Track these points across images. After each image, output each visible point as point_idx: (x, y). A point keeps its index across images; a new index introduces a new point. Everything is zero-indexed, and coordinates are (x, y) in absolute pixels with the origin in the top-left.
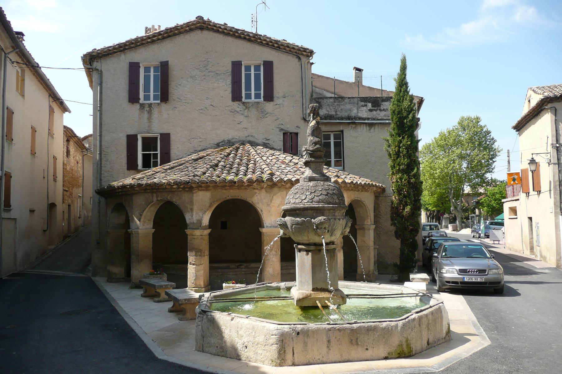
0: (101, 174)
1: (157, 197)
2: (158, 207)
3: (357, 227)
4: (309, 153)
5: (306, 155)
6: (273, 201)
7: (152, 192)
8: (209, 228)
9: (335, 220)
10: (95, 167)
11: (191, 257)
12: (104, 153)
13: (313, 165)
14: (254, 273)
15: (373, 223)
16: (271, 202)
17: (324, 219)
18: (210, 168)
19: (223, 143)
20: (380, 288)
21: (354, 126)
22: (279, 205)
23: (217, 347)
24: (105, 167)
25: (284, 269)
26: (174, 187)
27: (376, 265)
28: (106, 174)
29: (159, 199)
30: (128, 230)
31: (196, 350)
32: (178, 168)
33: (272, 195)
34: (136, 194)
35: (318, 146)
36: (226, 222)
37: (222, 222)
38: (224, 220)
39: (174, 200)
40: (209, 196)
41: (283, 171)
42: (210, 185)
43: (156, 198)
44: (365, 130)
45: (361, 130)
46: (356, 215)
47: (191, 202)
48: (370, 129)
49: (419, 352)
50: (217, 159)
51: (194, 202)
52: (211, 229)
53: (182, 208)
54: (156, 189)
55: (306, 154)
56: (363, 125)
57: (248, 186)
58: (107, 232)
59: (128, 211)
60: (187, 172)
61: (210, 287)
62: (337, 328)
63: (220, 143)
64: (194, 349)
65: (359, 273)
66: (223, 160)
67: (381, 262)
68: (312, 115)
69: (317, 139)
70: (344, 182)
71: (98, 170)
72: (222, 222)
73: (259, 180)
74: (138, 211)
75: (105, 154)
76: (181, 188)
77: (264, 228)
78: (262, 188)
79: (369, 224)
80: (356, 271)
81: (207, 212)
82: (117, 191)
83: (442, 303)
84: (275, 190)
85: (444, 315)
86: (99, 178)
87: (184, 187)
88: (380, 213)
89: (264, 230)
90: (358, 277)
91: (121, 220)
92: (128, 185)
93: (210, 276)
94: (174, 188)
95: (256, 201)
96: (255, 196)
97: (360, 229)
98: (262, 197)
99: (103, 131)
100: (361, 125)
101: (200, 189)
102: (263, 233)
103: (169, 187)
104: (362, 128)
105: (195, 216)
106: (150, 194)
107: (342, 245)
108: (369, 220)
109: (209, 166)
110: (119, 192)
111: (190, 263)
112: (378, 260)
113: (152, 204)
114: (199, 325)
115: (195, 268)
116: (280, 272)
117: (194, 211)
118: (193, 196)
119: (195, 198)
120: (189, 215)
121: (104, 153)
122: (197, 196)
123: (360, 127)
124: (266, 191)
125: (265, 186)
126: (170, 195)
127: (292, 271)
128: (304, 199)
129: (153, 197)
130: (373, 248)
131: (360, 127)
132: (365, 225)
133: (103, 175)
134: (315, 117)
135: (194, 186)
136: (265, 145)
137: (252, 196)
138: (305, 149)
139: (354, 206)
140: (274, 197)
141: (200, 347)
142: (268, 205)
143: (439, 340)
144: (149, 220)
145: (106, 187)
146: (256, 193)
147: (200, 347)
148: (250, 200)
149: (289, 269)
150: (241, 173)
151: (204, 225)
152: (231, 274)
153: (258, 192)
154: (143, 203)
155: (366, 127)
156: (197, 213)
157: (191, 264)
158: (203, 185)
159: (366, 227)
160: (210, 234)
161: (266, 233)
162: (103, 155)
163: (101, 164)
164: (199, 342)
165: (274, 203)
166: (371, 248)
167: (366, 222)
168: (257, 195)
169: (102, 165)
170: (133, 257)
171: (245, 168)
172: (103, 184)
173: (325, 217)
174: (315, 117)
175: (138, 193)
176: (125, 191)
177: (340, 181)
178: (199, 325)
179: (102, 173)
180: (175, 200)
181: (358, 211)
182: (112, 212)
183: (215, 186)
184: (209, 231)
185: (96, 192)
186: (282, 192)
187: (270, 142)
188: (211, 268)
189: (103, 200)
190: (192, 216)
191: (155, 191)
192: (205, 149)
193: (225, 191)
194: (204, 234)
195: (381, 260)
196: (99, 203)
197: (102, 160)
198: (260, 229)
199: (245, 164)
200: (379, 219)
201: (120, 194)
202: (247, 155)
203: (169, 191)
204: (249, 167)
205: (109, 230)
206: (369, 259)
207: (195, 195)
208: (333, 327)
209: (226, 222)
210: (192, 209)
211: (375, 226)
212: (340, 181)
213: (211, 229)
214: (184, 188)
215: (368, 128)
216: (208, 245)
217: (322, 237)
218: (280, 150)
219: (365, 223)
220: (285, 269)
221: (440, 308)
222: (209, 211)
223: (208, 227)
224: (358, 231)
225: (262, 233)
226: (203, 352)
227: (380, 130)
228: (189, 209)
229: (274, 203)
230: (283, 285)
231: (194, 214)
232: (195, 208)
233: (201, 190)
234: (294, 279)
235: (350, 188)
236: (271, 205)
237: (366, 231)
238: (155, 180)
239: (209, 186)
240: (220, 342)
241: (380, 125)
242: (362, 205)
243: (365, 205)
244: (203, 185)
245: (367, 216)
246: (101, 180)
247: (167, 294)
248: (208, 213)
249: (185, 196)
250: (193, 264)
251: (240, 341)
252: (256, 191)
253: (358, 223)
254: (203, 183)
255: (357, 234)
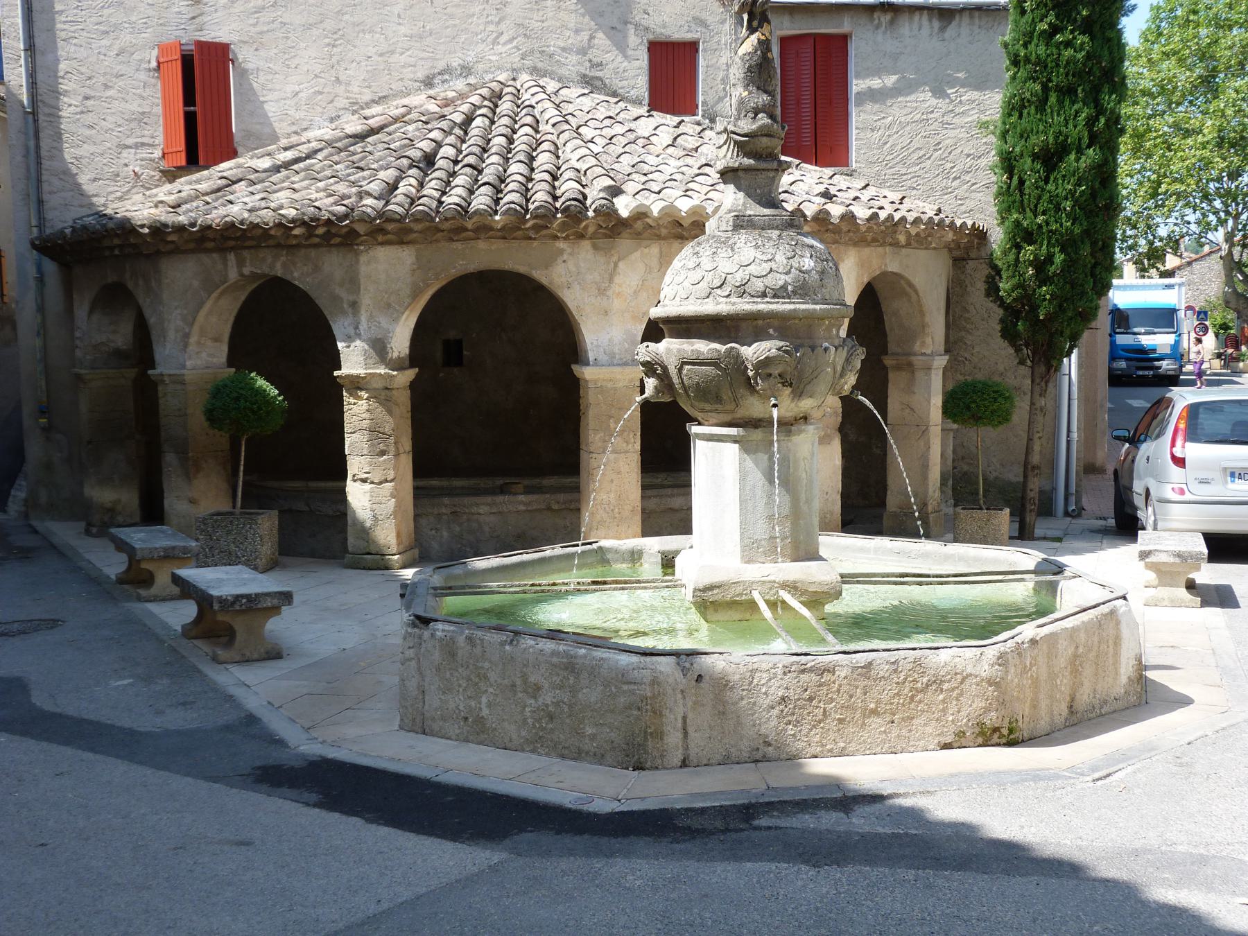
0: (39, 181)
1: (241, 263)
2: (243, 298)
3: (888, 361)
4: (736, 142)
5: (726, 146)
6: (617, 279)
7: (222, 250)
8: (412, 366)
9: (813, 351)
10: (19, 158)
11: (357, 458)
12: (47, 110)
13: (745, 179)
14: (555, 507)
15: (942, 349)
16: (611, 280)
17: (779, 349)
18: (411, 166)
19: (446, 77)
20: (947, 558)
21: (888, 17)
22: (635, 292)
23: (466, 719)
24: (52, 158)
25: (650, 497)
26: (296, 232)
27: (950, 482)
28: (55, 181)
29: (246, 271)
30: (150, 372)
31: (401, 728)
32: (301, 165)
33: (615, 259)
34: (171, 253)
35: (763, 119)
36: (459, 343)
37: (447, 343)
38: (452, 334)
39: (296, 274)
40: (409, 262)
41: (650, 176)
42: (412, 225)
43: (235, 270)
44: (926, 31)
45: (911, 30)
46: (887, 324)
47: (353, 283)
48: (943, 29)
49: (1043, 733)
50: (431, 135)
51: (362, 281)
52: (417, 370)
53: (322, 302)
54: (236, 239)
55: (725, 143)
56: (921, 15)
57: (536, 228)
58: (78, 377)
59: (147, 313)
60: (332, 180)
61: (416, 551)
62: (809, 665)
63: (434, 76)
64: (397, 727)
65: (893, 510)
66: (451, 139)
67: (965, 473)
68: (746, 17)
69: (763, 98)
70: (849, 217)
71: (28, 170)
72: (447, 343)
73: (572, 208)
74: (178, 311)
75: (50, 115)
76: (317, 236)
77: (588, 364)
78: (581, 236)
79: (929, 352)
80: (883, 504)
81: (405, 316)
82: (106, 243)
83: (1124, 598)
84: (624, 243)
85: (1125, 632)
86: (33, 198)
87: (328, 231)
88: (967, 315)
89: (587, 373)
90: (886, 522)
91: (121, 336)
92: (143, 226)
93: (416, 517)
94: (296, 236)
95: (563, 279)
96: (559, 261)
97: (899, 368)
98: (582, 265)
99: (36, 34)
100: (914, 12)
101: (380, 238)
102: (586, 381)
103: (279, 234)
104: (915, 26)
105: (365, 326)
106: (215, 255)
107: (840, 419)
108: (929, 340)
109: (405, 162)
110: (112, 248)
111: (354, 476)
112: (954, 468)
113: (222, 288)
114: (410, 660)
115: (372, 491)
116: (639, 504)
117: (363, 312)
118: (358, 261)
119: (363, 269)
120: (346, 323)
121: (47, 110)
122: (369, 262)
123: (911, 19)
124: (595, 247)
125: (591, 230)
126: (283, 258)
127: (677, 502)
128: (720, 287)
129: (226, 265)
130: (939, 428)
131: (911, 19)
132: (915, 355)
133: (45, 187)
134: (755, 24)
135: (361, 228)
136: (587, 83)
137: (548, 264)
138: (722, 129)
139: (882, 293)
140: (621, 265)
141: (414, 720)
142: (602, 292)
143: (1106, 702)
144: (216, 340)
145: (68, 231)
146: (561, 252)
147: (414, 720)
148: (540, 276)
149: (669, 496)
150: (512, 186)
151: (395, 355)
152: (481, 511)
153: (569, 250)
154: (196, 283)
155: (930, 20)
156: (371, 318)
157: (355, 481)
158: (390, 227)
159: (917, 361)
160: (413, 385)
161: (596, 381)
162: (41, 118)
163: (38, 147)
164: (412, 705)
165: (620, 286)
166: (932, 429)
167: (918, 344)
168: (565, 257)
169: (43, 153)
170: (170, 458)
171: (521, 168)
172: (49, 215)
173: (782, 343)
174: (755, 24)
175: (177, 251)
176: (134, 246)
177: (836, 210)
178: (410, 660)
179: (44, 178)
180: (300, 274)
181: (893, 309)
182: (91, 312)
183: (428, 229)
184: (411, 374)
185: (34, 246)
186: (646, 251)
187: (605, 74)
188: (418, 493)
189: (50, 267)
190: (357, 328)
191: (232, 243)
192: (385, 97)
193: (459, 245)
194: (395, 386)
195: (966, 468)
196: (41, 280)
197: (41, 135)
198: (575, 368)
199: (523, 154)
200: (963, 334)
201: (117, 252)
202: (529, 120)
203: (279, 246)
204: (535, 164)
205: (83, 371)
206: (925, 467)
207: (363, 258)
208: (798, 663)
209: (459, 343)
210: (354, 305)
211: (947, 357)
212: (836, 210)
213: (417, 370)
214: (328, 236)
215: (936, 24)
216: (409, 422)
217: (773, 402)
218: (637, 102)
219: (917, 347)
220: (655, 496)
221: (1113, 612)
222: (411, 311)
223: (407, 363)
224: (891, 375)
225: (582, 383)
226: (424, 733)
227: (977, 30)
228: (345, 306)
229: (620, 286)
230: (655, 545)
231: (363, 318)
232: (366, 301)
233: (382, 244)
234: (684, 527)
235: (869, 236)
236: (610, 293)
237: (920, 375)
238: (235, 210)
239: (411, 231)
240: (473, 704)
241: (977, 14)
242: (908, 289)
243: (916, 291)
244: (390, 227)
245: (923, 327)
246: (40, 202)
247: (177, 580)
248: (408, 316)
249: (333, 263)
250: (364, 481)
251: (532, 701)
252: (561, 245)
253: (892, 347)
254: (389, 220)
255: (890, 385)
